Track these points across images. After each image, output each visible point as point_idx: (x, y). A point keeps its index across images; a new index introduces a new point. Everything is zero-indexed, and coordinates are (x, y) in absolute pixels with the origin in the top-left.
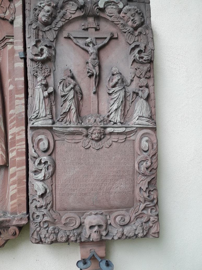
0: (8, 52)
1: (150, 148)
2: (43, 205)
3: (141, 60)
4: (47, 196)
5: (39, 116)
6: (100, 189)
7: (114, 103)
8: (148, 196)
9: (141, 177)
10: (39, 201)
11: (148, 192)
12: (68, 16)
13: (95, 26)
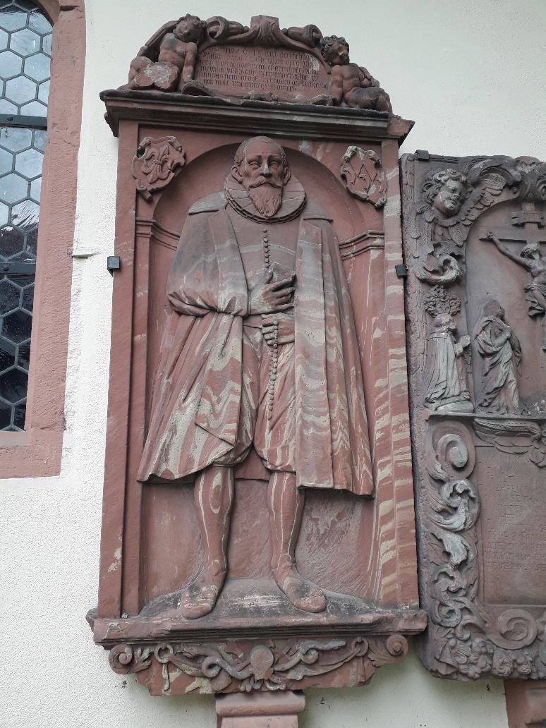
0: (372, 263)
2: (463, 587)
4: (468, 567)
5: (446, 393)
12: (490, 200)
13: (538, 220)
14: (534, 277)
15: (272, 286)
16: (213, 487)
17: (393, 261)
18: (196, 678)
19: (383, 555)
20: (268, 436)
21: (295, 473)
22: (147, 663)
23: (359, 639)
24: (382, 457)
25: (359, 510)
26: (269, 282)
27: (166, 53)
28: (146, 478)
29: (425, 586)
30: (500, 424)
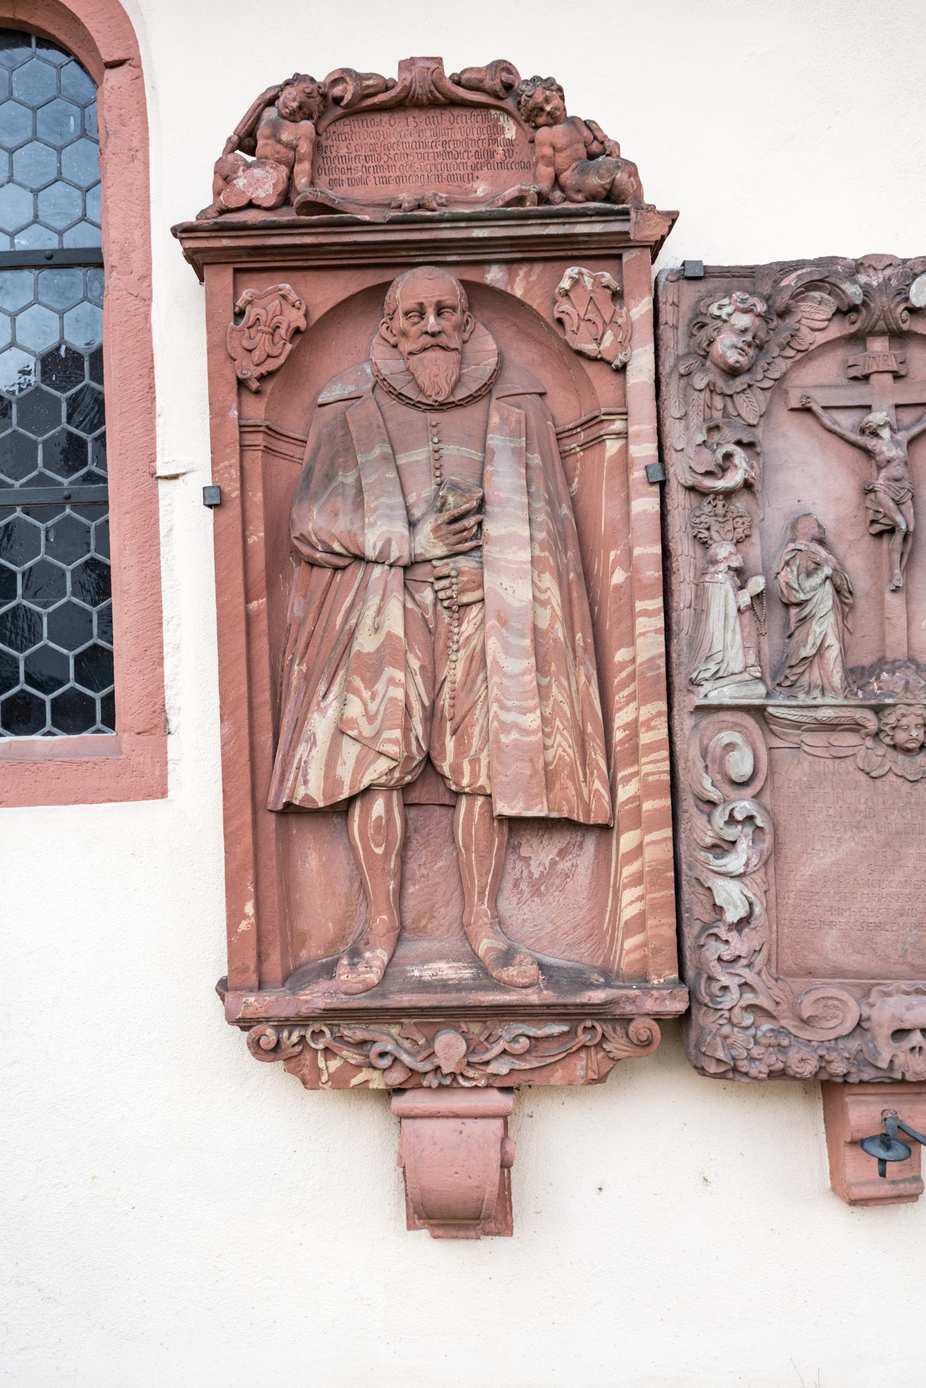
0: (609, 463)
2: (743, 954)
4: (752, 926)
10: (727, 942)
13: (895, 368)
14: (880, 468)
15: (446, 516)
16: (373, 819)
18: (364, 1069)
19: (625, 907)
20: (450, 744)
21: (490, 796)
22: (298, 1049)
23: (589, 1024)
24: (625, 767)
25: (590, 844)
26: (440, 510)
27: (266, 145)
28: (280, 807)
29: (688, 953)
30: (810, 714)
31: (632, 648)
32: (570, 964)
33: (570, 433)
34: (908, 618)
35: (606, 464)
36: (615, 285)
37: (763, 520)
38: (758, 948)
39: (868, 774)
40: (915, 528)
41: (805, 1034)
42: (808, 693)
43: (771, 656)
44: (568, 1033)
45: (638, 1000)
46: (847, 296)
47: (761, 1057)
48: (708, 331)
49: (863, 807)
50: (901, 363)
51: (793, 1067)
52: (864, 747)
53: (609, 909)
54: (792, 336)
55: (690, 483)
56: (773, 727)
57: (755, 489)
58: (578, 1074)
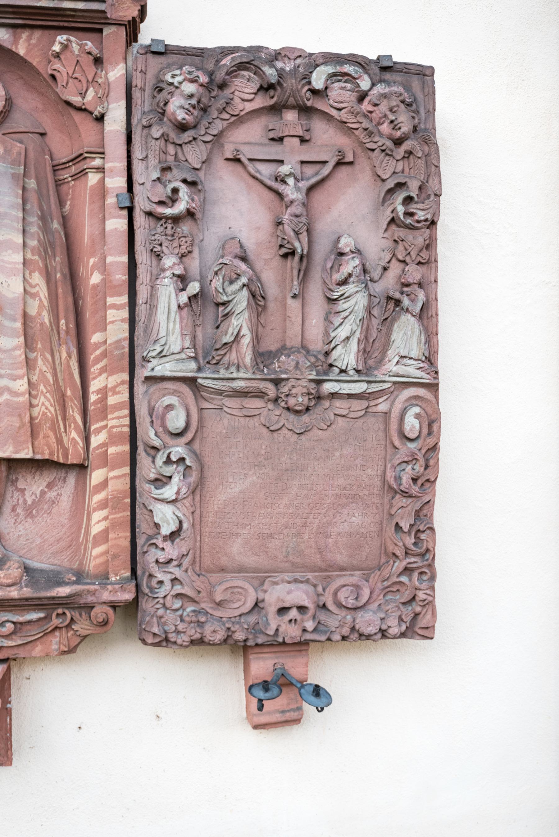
0: (90, 191)
1: (425, 431)
2: (174, 558)
3: (409, 221)
4: (181, 537)
6: (305, 525)
7: (342, 322)
8: (415, 544)
9: (398, 500)
10: (163, 549)
11: (413, 534)
13: (301, 134)
17: (113, 188)
19: (94, 525)
23: (60, 611)
24: (97, 421)
25: (71, 479)
30: (228, 384)
31: (104, 332)
32: (53, 567)
33: (65, 165)
34: (303, 317)
35: (88, 192)
36: (95, 51)
37: (202, 240)
38: (185, 553)
39: (268, 428)
40: (308, 252)
41: (218, 613)
42: (227, 369)
43: (204, 341)
44: (45, 618)
45: (97, 593)
46: (266, 76)
47: (184, 630)
48: (164, 94)
49: (263, 452)
50: (307, 130)
51: (208, 636)
52: (266, 409)
53: (84, 526)
54: (227, 103)
55: (148, 209)
56: (203, 394)
57: (196, 217)
58: (53, 647)
